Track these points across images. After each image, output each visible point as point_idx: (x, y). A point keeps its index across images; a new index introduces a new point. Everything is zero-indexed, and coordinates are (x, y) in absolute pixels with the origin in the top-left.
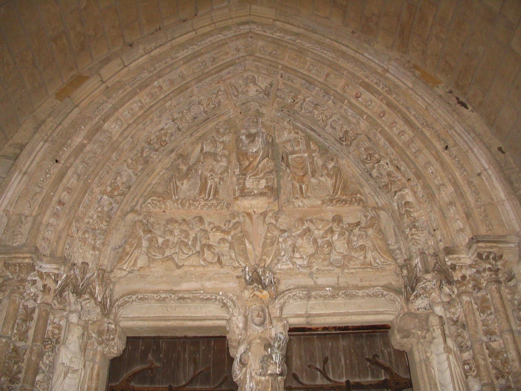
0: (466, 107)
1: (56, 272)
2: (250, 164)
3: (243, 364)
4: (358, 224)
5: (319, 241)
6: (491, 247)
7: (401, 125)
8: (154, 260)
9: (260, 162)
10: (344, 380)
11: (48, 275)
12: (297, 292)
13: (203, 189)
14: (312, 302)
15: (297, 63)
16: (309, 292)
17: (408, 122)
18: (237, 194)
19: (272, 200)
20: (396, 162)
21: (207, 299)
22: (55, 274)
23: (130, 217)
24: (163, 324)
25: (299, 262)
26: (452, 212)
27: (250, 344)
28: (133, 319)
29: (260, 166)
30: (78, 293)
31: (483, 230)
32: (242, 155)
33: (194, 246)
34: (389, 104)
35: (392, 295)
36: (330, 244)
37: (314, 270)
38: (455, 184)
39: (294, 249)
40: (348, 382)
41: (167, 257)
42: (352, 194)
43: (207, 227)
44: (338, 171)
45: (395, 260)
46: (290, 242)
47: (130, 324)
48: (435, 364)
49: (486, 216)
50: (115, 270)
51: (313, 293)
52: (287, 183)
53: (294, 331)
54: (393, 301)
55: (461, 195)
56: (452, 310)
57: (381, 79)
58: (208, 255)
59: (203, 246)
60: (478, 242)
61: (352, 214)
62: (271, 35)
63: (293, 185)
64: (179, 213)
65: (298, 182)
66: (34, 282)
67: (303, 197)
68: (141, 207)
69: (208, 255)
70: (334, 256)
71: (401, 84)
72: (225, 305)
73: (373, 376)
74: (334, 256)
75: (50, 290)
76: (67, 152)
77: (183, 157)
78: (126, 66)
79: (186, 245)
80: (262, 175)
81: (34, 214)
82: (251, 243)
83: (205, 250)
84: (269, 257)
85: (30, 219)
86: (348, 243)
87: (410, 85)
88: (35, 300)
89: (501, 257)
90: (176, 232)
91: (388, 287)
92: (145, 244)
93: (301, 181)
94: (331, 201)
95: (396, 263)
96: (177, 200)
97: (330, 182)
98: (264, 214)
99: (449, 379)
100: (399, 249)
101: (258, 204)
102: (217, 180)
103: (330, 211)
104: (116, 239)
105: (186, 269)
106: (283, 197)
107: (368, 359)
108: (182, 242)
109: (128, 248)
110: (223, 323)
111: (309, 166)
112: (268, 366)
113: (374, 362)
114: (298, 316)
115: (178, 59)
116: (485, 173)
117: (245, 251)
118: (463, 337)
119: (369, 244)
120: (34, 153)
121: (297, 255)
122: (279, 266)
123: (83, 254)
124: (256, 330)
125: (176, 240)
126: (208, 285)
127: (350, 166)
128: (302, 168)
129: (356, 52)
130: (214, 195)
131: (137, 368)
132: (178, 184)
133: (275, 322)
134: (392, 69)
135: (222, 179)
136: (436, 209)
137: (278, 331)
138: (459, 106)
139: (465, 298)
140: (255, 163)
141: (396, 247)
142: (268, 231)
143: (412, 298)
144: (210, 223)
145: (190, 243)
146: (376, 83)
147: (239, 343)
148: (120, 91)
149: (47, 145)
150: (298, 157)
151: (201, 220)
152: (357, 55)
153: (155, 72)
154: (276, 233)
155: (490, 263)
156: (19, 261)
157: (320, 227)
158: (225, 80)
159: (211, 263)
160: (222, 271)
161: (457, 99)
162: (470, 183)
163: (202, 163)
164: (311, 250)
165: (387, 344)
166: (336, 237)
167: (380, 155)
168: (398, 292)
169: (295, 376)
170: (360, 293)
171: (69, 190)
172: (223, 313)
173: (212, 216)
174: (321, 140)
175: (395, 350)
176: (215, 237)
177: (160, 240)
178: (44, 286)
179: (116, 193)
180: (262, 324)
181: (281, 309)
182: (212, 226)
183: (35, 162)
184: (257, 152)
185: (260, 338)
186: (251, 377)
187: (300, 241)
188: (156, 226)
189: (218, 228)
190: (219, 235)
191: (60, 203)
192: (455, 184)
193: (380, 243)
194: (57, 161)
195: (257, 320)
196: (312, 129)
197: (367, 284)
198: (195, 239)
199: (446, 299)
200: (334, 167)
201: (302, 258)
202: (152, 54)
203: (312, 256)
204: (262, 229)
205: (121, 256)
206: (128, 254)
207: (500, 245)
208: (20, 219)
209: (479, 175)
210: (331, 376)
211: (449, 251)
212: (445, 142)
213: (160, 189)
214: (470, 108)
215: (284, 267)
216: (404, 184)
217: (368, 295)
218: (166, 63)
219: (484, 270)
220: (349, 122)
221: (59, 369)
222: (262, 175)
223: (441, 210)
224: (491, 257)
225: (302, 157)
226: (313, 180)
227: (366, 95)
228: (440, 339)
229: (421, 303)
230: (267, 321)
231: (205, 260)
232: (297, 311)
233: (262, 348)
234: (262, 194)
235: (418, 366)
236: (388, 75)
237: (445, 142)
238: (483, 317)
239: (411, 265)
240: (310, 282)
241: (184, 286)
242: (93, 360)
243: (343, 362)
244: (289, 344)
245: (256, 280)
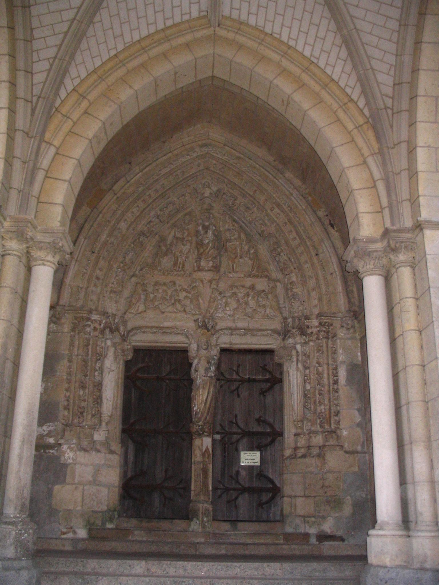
0: (334, 228)
1: (100, 319)
2: (204, 251)
3: (196, 371)
4: (264, 291)
5: (241, 300)
6: (327, 319)
7: (294, 234)
8: (148, 309)
9: (209, 251)
10: (247, 377)
11: (96, 321)
12: (225, 331)
13: (175, 264)
14: (233, 337)
15: (237, 179)
16: (232, 330)
17: (298, 233)
18: (196, 269)
19: (215, 273)
20: (289, 256)
21: (178, 334)
22: (99, 321)
23: (134, 279)
24: (154, 344)
25: (229, 312)
26: (313, 294)
27: (200, 360)
28: (138, 342)
29: (210, 253)
30: (112, 331)
31: (326, 309)
32: (200, 245)
33: (171, 299)
34: (290, 220)
35: (276, 336)
36: (247, 303)
37: (236, 318)
38: (317, 279)
39: (227, 304)
40: (249, 378)
41: (155, 306)
42: (262, 272)
43: (177, 288)
44: (256, 253)
45: (281, 313)
46: (224, 301)
47: (137, 344)
48: (291, 374)
49: (329, 301)
50: (127, 313)
51: (234, 332)
52: (225, 262)
53: (224, 351)
54: (276, 339)
55: (319, 287)
56: (305, 348)
57: (287, 201)
58: (179, 306)
59: (176, 300)
60: (320, 316)
61: (261, 284)
62: (221, 157)
63: (228, 263)
64: (162, 279)
65: (232, 262)
66: (90, 326)
67: (234, 272)
68: (139, 272)
69: (179, 306)
70: (249, 310)
71: (299, 205)
72: (187, 337)
73: (262, 376)
74: (249, 310)
75: (97, 329)
76: (98, 245)
77: (163, 239)
78: (128, 182)
79: (166, 299)
80: (210, 259)
81: (85, 286)
82: (202, 300)
83: (177, 303)
84: (212, 309)
85: (84, 290)
86: (257, 303)
87: (304, 207)
88: (90, 335)
89: (332, 325)
90: (160, 291)
91: (274, 331)
92: (143, 297)
93: (233, 262)
94: (250, 276)
95: (282, 315)
96: (161, 270)
97: (250, 263)
98: (210, 281)
99: (295, 383)
100: (285, 307)
101: (207, 276)
102: (184, 258)
103: (248, 282)
104: (126, 293)
105: (166, 314)
106: (222, 270)
107: (261, 367)
108: (164, 298)
109: (134, 301)
110: (186, 345)
111: (239, 251)
112: (208, 373)
113: (264, 369)
114: (227, 344)
115: (161, 175)
116: (334, 273)
117: (199, 305)
118: (307, 363)
119: (268, 303)
120: (80, 247)
121: (228, 309)
122: (217, 315)
123: (111, 307)
124: (203, 352)
125: (160, 295)
126: (178, 324)
127: (263, 249)
128: (234, 253)
129: (275, 177)
130: (182, 268)
131: (140, 365)
132: (161, 259)
133: (213, 348)
134: (294, 195)
135: (187, 257)
136: (305, 291)
137: (215, 352)
138: (329, 226)
139: (311, 343)
140: (207, 251)
141: (283, 306)
142: (212, 293)
143: (287, 337)
144: (180, 286)
145: (168, 298)
146: (284, 203)
147: (194, 358)
148: (126, 201)
149: (86, 241)
150: (233, 245)
151: (174, 283)
152: (275, 180)
153: (147, 186)
154: (217, 294)
155: (325, 328)
156: (81, 315)
157: (242, 291)
158: (189, 186)
159: (180, 311)
160: (186, 316)
161: (330, 221)
162: (325, 279)
163: (176, 246)
164: (235, 306)
165: (272, 359)
166: (250, 298)
167: (281, 249)
168: (279, 334)
169: (222, 374)
170: (259, 334)
171: (101, 269)
172: (186, 340)
173: (182, 282)
174: (248, 230)
175: (276, 363)
176: (182, 295)
177: (152, 296)
178: (95, 327)
179: (126, 268)
180: (206, 349)
181: (217, 340)
182: (181, 287)
183: (81, 253)
184: (208, 242)
185: (205, 357)
186: (200, 377)
187: (230, 300)
188: (148, 286)
189: (184, 290)
190: (185, 294)
191: (98, 278)
192: (317, 279)
193: (274, 304)
194: (93, 252)
195: (204, 347)
196: (243, 222)
197: (264, 328)
198: (171, 297)
199: (303, 342)
200: (254, 252)
201: (230, 310)
202: (144, 171)
203: (236, 309)
204: (209, 291)
205: (130, 305)
206: (134, 304)
207: (332, 318)
208: (78, 289)
209: (332, 274)
210: (241, 374)
211: (307, 318)
212: (317, 251)
213: (150, 261)
214: (336, 229)
215: (220, 315)
216: (292, 270)
217: (263, 335)
218: (153, 178)
219: (322, 331)
220: (265, 225)
221: (106, 370)
222: (210, 259)
223: (308, 291)
224: (326, 324)
225: (235, 245)
226: (241, 260)
227: (276, 210)
228: (295, 363)
229: (290, 341)
230: (209, 347)
231: (176, 309)
232: (225, 340)
233: (206, 363)
234: (210, 270)
235: (285, 374)
236: (292, 197)
237: (317, 251)
238: (318, 354)
239: (287, 322)
240: (233, 325)
241: (166, 324)
242: (119, 363)
243: (248, 368)
244: (220, 359)
245: (205, 326)
